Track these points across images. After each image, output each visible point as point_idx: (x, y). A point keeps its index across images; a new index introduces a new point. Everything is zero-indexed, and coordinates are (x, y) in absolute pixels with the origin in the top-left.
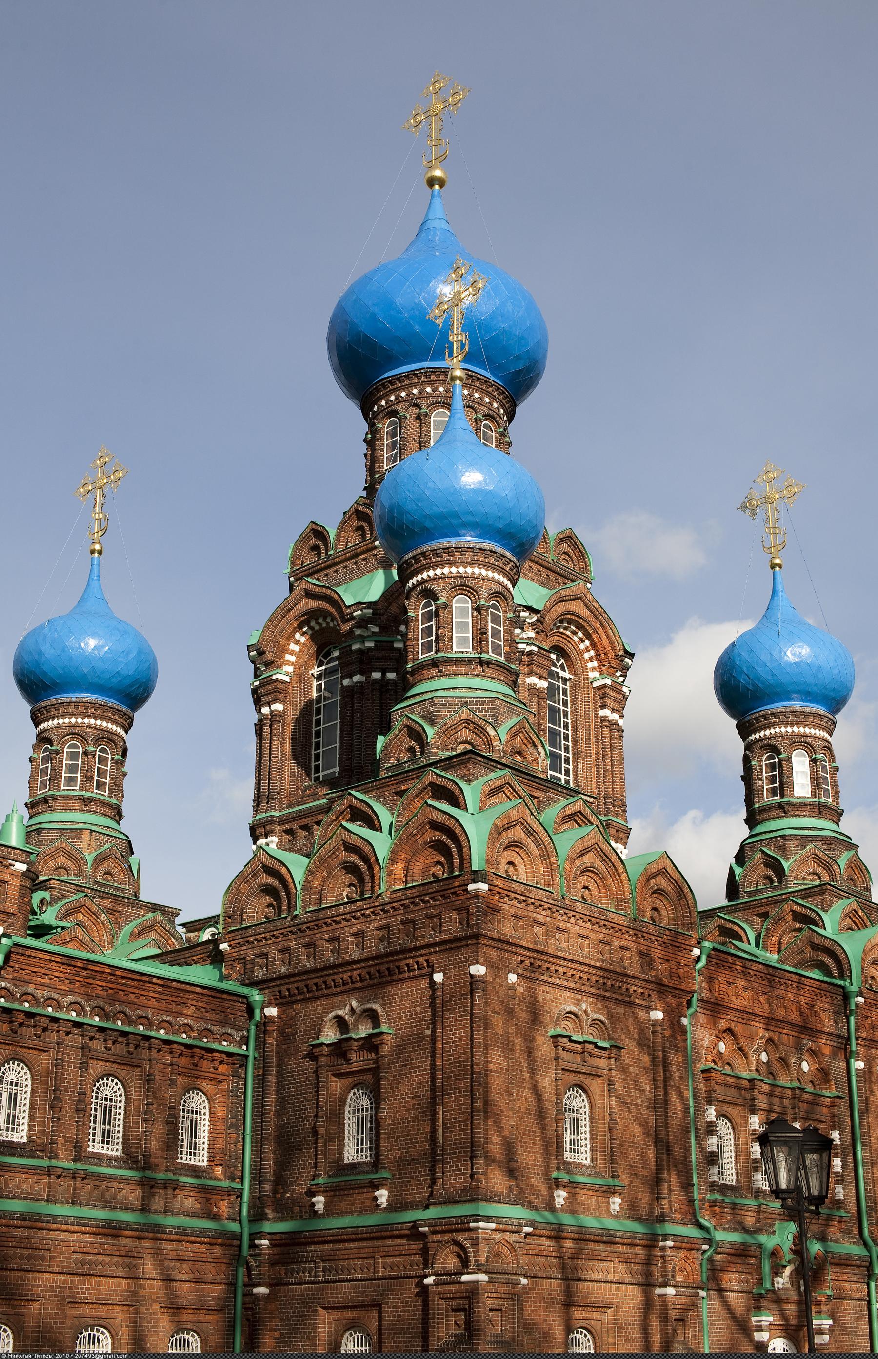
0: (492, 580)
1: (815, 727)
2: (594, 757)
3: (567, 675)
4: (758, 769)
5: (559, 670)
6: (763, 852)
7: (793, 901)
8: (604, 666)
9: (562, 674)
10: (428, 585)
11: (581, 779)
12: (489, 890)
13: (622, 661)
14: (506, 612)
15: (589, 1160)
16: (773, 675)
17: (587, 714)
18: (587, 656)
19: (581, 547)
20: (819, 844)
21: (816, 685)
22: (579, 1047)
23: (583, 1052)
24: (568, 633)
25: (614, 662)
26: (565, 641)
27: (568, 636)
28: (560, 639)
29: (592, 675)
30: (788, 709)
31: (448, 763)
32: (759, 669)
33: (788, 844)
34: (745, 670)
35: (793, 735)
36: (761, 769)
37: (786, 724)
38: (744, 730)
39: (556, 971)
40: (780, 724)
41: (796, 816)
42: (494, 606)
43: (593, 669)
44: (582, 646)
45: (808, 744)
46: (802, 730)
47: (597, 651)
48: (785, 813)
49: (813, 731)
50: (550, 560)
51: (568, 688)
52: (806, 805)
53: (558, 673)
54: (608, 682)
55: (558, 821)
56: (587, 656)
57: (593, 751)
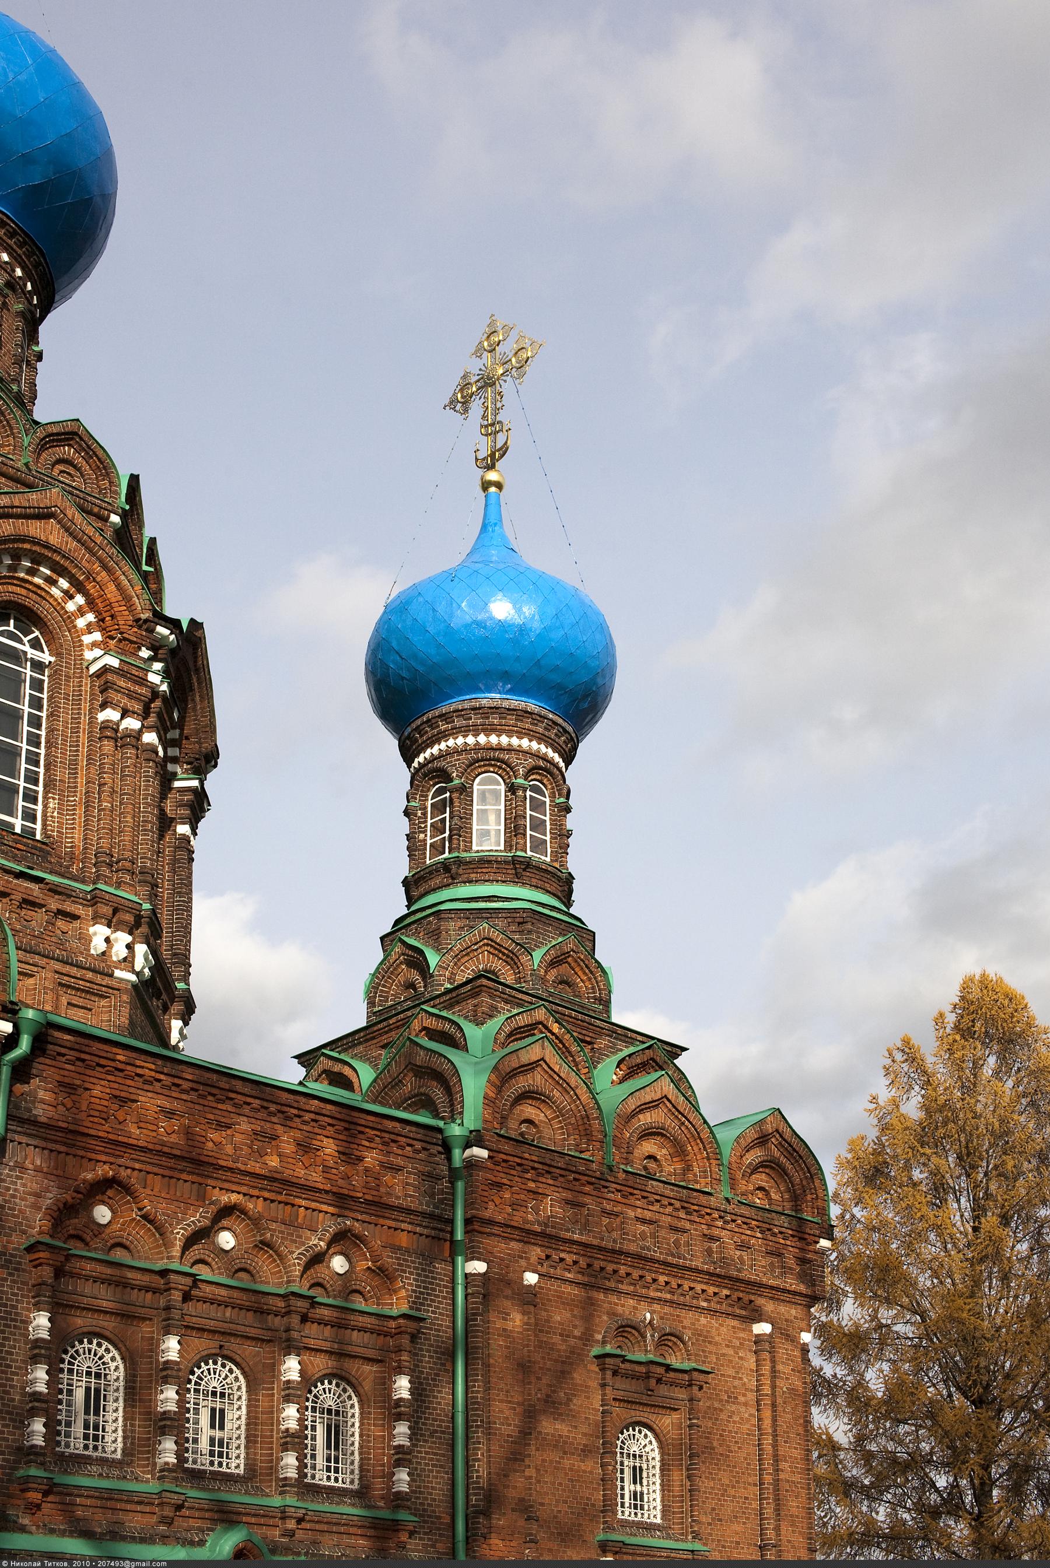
0: (528, 753)
1: (520, 735)
2: (81, 788)
3: (46, 657)
4: (419, 813)
5: (27, 648)
6: (404, 943)
7: (426, 1012)
8: (112, 638)
9: (32, 653)
10: (442, 764)
11: (53, 825)
12: (489, 1157)
13: (152, 631)
14: (552, 796)
15: (659, 1516)
16: (439, 646)
17: (76, 720)
18: (81, 623)
19: (100, 453)
20: (501, 923)
21: (518, 659)
22: (643, 1369)
23: (690, 1385)
24: (37, 580)
25: (132, 633)
26: (34, 597)
27: (38, 587)
28: (24, 592)
29: (89, 655)
30: (467, 705)
31: (454, 997)
32: (416, 639)
33: (444, 925)
34: (394, 644)
35: (477, 747)
36: (425, 814)
37: (465, 731)
38: (408, 753)
39: (562, 1260)
40: (455, 732)
41: (470, 882)
42: (535, 789)
43: (94, 645)
44: (71, 606)
45: (503, 761)
46: (494, 739)
47: (98, 613)
48: (453, 878)
49: (515, 741)
50: (19, 465)
51: (46, 679)
52: (489, 862)
53: (25, 653)
54: (115, 662)
55: (502, 1036)
56: (81, 623)
57: (81, 780)
